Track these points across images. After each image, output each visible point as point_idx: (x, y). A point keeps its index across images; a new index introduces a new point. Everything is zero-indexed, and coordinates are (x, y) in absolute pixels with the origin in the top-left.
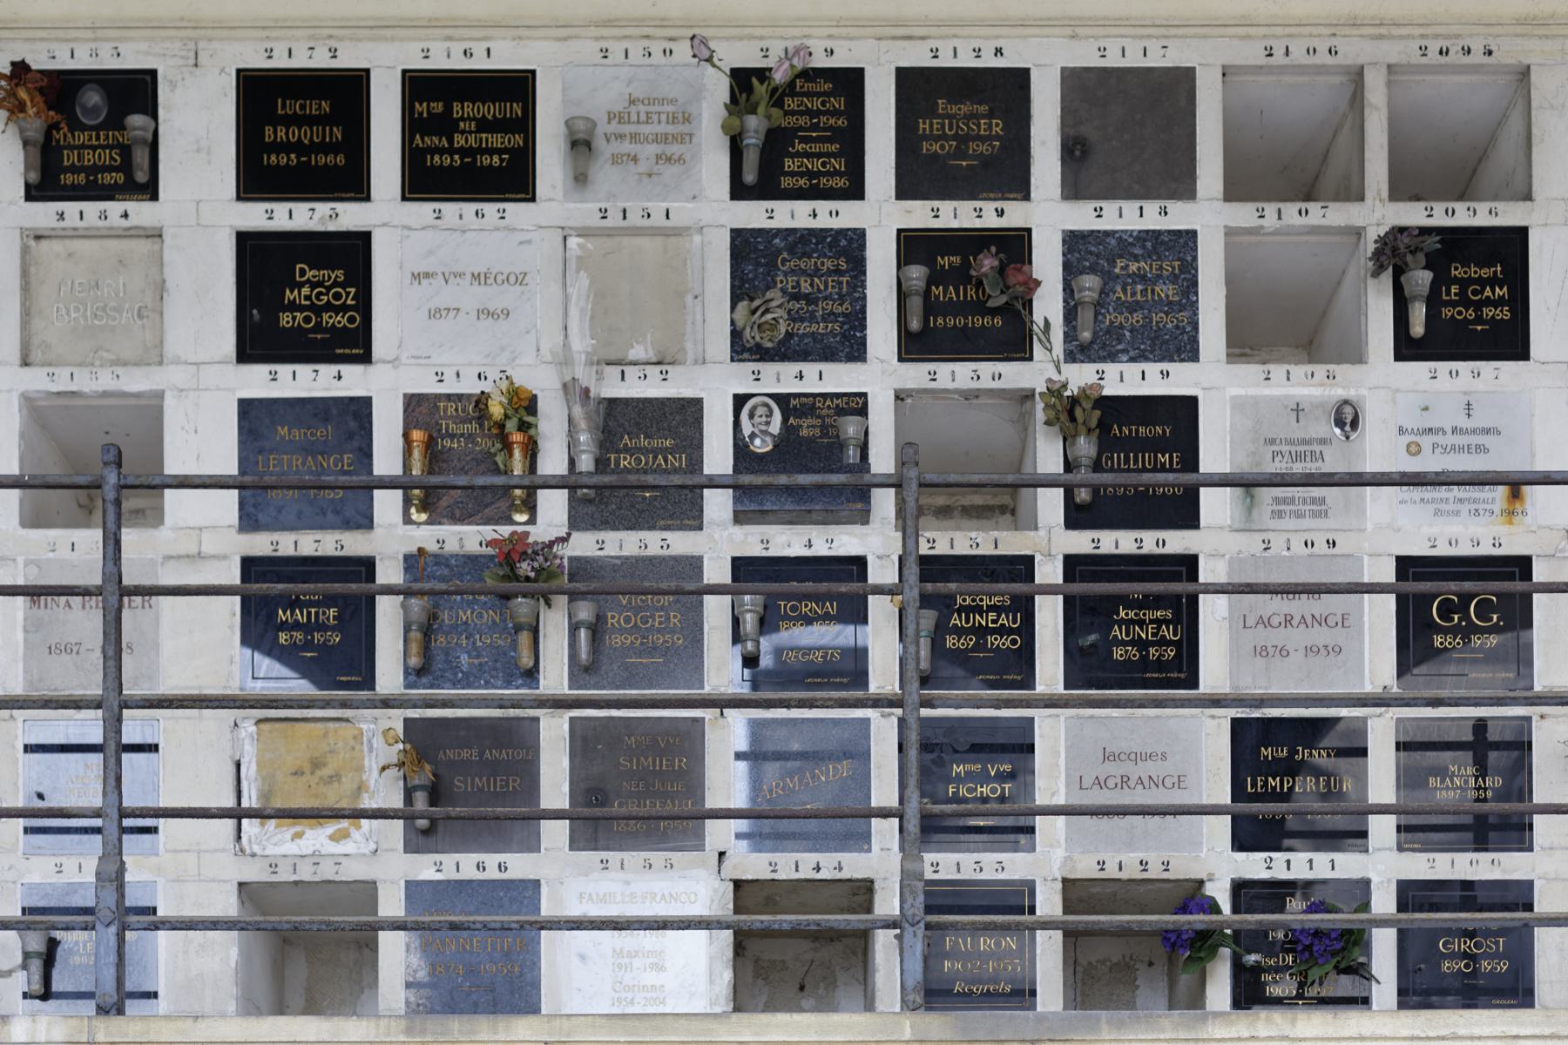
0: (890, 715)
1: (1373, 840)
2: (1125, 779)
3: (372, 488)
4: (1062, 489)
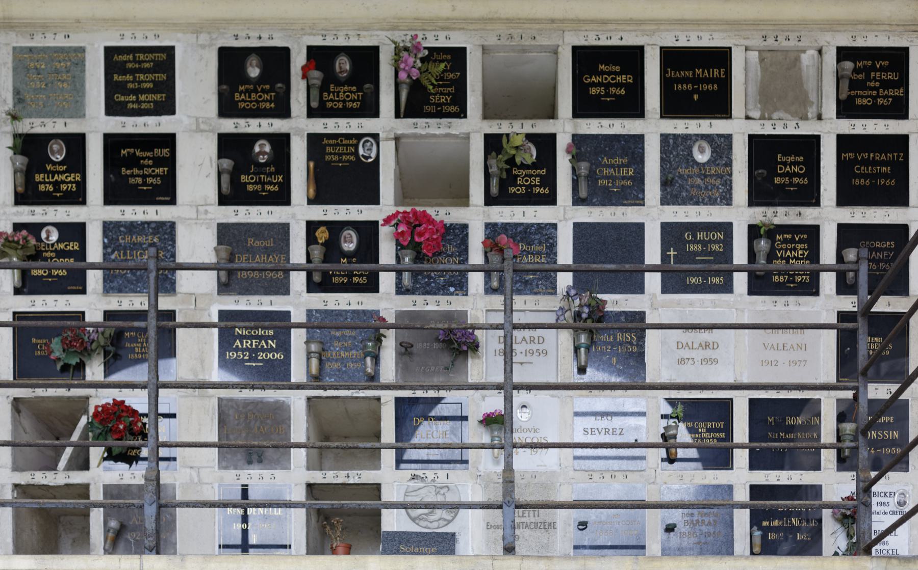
0: (210, 397)
2: (607, 430)
4: (746, 273)
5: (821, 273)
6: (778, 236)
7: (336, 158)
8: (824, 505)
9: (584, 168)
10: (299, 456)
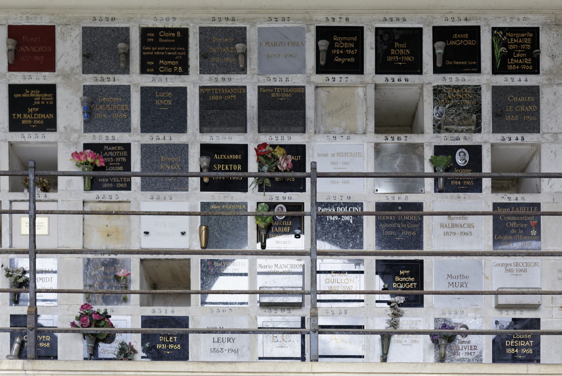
1: (193, 303)
3: (188, 177)
8: (117, 331)
10: (135, 299)
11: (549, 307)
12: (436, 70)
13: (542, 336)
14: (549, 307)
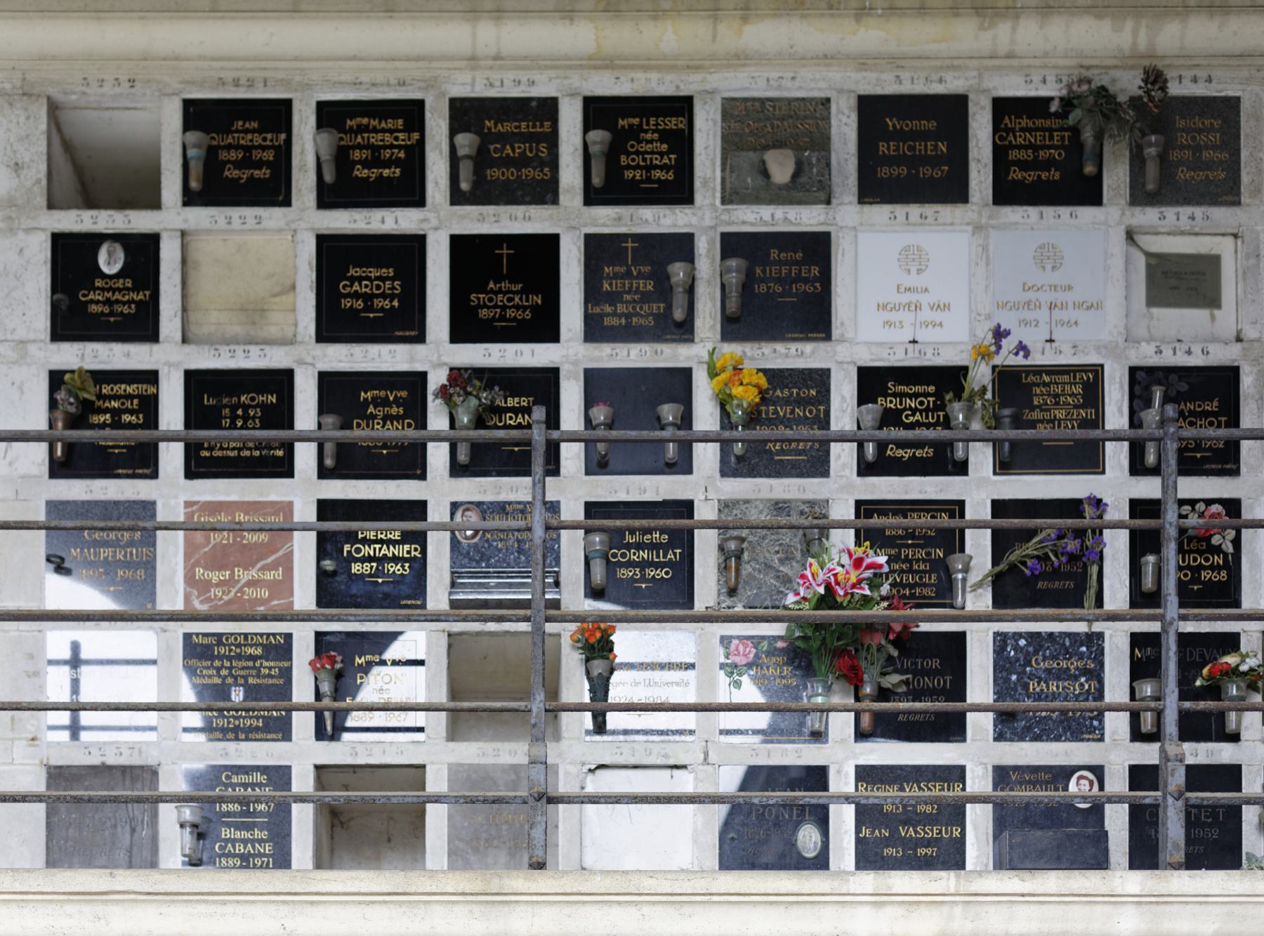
4: (856, 444)
5: (694, 444)
6: (363, 394)
7: (359, 304)
9: (466, 142)
11: (5, 739)
12: (457, 197)
13: (429, 807)
14: (5, 739)
